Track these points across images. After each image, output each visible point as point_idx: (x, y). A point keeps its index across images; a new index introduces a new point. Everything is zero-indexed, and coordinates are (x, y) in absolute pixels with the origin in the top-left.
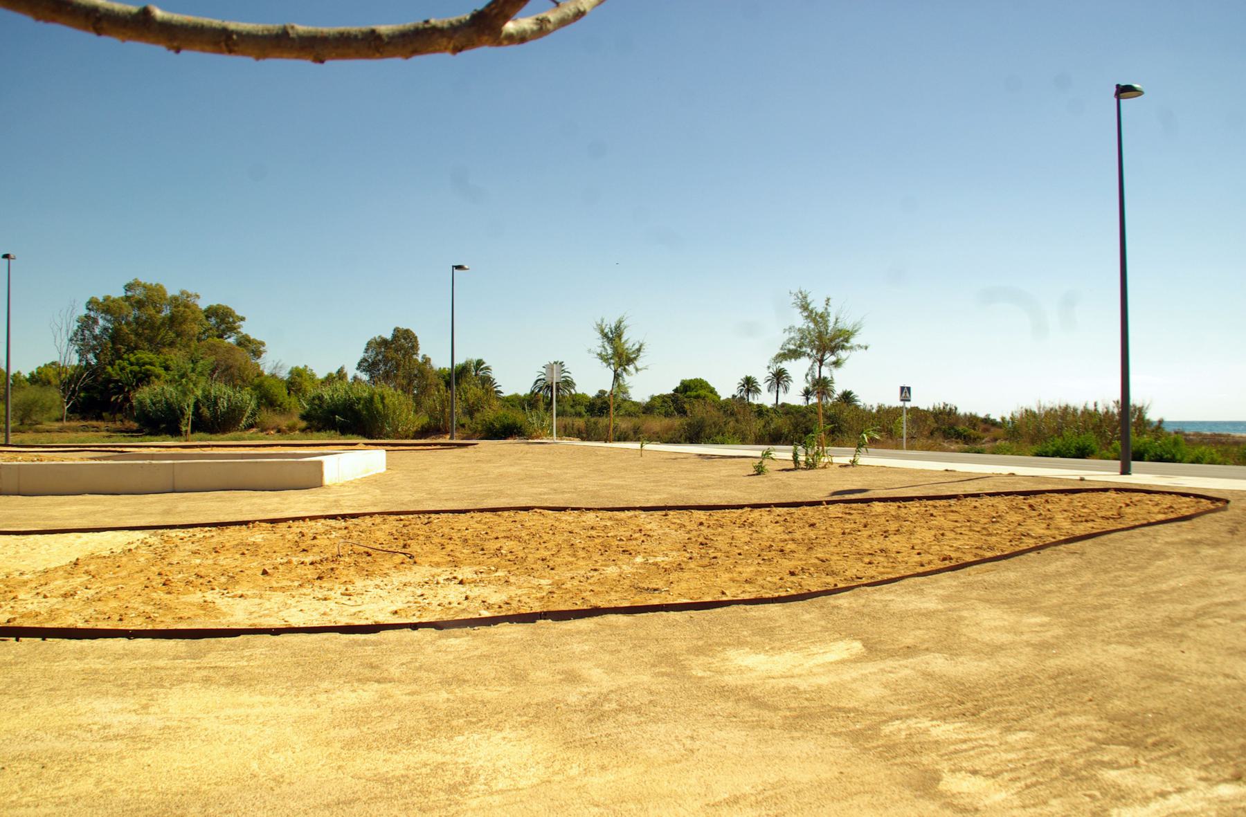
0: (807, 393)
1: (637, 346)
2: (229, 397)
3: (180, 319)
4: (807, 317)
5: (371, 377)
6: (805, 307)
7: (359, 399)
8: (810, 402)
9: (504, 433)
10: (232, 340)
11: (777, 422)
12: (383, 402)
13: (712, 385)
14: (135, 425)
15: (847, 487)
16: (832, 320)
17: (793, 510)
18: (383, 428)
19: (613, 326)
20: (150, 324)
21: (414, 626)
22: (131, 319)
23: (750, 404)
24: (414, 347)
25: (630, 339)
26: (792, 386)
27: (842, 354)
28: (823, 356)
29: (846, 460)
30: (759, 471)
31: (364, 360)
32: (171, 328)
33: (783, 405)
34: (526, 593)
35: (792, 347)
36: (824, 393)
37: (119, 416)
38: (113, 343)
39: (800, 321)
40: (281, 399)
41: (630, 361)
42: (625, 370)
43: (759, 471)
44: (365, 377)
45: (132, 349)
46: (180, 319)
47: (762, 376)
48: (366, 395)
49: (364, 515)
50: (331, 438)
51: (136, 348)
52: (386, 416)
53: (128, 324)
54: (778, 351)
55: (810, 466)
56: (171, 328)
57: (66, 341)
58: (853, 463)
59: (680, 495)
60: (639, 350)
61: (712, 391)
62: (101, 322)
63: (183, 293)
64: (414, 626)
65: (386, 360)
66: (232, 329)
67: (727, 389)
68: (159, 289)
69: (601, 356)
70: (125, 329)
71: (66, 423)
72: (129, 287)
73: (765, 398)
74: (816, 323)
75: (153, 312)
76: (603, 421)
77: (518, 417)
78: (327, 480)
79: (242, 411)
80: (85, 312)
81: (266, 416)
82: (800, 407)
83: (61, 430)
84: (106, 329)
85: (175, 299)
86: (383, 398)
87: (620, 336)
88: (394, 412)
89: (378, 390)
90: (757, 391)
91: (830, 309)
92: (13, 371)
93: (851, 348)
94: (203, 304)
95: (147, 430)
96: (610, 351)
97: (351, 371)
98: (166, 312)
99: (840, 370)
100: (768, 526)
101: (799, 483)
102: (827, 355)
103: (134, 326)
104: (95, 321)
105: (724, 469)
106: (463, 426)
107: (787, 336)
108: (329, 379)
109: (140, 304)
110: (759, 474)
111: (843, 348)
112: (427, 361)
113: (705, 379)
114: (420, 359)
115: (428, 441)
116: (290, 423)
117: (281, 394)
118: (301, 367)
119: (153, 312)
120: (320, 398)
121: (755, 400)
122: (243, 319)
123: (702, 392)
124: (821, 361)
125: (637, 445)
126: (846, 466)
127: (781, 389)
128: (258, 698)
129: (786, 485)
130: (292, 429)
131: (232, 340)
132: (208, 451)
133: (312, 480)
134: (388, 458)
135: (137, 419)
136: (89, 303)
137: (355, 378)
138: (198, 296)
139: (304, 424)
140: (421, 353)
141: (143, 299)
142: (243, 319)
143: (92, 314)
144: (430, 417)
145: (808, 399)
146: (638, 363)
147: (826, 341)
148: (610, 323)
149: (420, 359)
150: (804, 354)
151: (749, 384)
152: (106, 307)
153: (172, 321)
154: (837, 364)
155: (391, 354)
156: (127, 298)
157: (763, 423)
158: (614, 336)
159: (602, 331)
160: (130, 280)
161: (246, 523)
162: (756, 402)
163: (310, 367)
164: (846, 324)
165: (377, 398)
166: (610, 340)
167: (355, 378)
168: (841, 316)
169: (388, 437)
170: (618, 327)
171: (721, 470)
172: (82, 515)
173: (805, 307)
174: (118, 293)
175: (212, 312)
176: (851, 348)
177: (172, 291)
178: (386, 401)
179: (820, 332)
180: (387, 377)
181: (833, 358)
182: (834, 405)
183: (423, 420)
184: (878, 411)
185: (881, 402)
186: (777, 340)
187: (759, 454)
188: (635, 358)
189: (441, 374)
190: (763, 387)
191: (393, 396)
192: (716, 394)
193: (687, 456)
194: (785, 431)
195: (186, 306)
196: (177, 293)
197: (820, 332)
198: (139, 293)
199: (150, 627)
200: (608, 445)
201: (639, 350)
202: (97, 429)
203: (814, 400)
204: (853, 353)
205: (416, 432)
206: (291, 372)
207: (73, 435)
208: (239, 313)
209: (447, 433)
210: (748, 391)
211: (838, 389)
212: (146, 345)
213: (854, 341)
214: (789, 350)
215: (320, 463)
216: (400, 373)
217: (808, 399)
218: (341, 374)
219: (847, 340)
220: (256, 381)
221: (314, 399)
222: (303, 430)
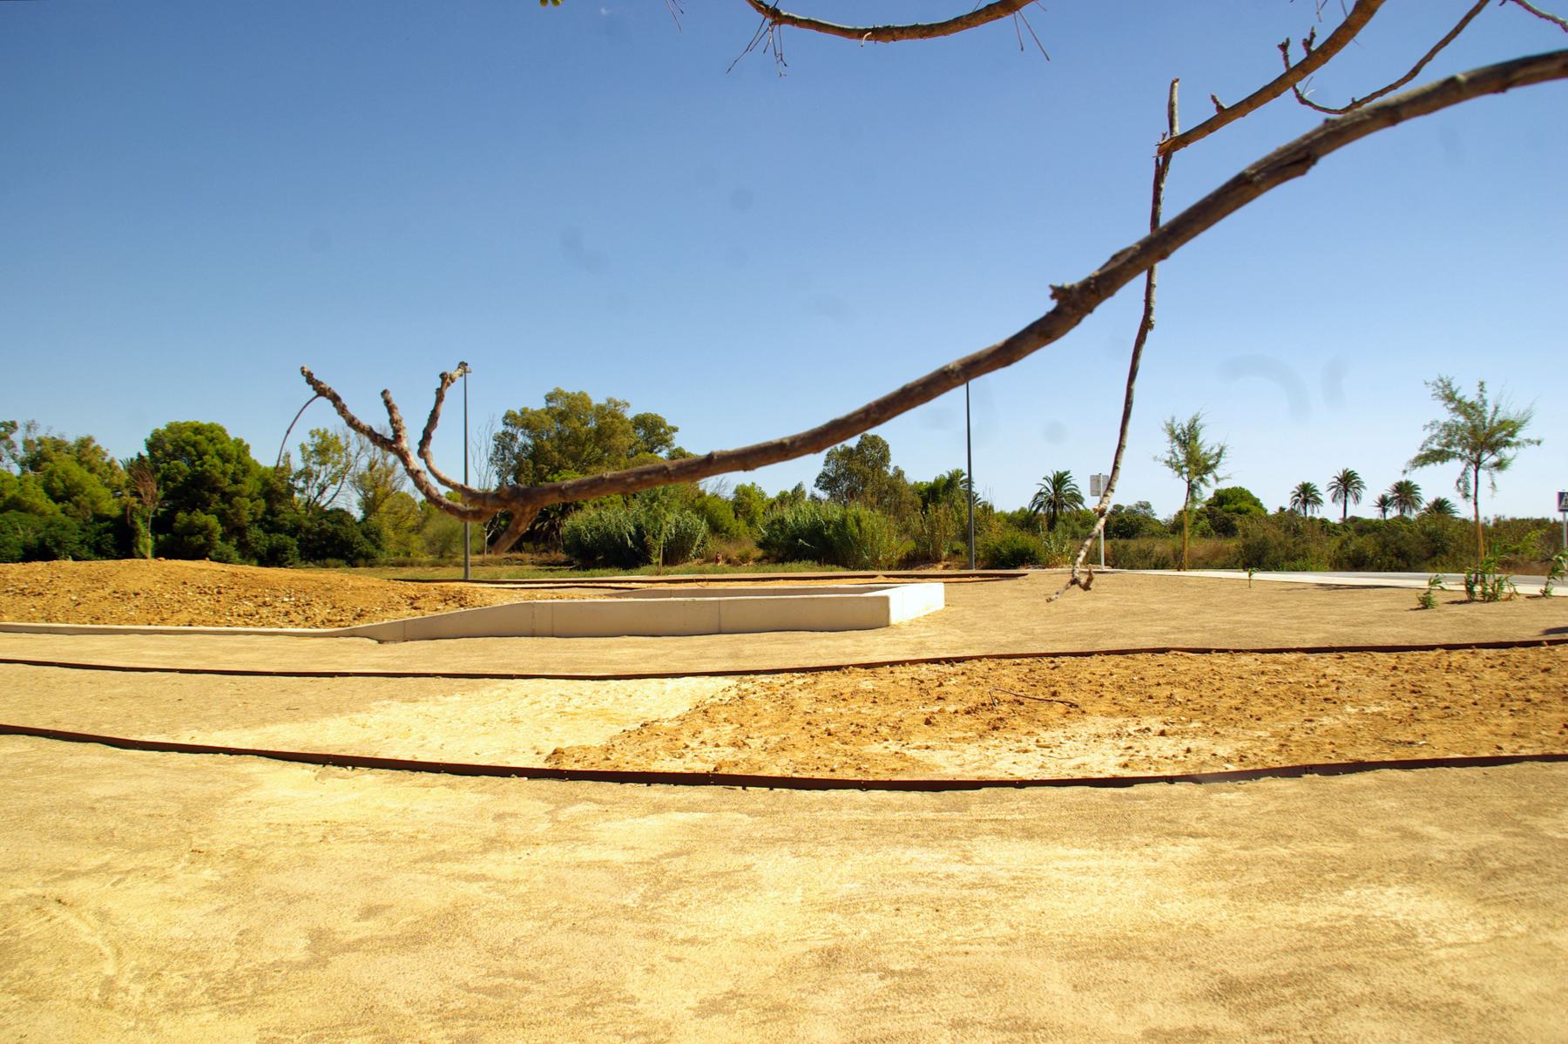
0: (1384, 503)
1: (1216, 450)
2: (678, 522)
3: (608, 432)
4: (1454, 410)
5: (832, 495)
6: (1450, 397)
7: (828, 523)
8: (1389, 516)
9: (1013, 560)
10: (664, 454)
11: (1357, 543)
12: (858, 525)
13: (1256, 495)
14: (562, 557)
15: (268, 639)
16: (1490, 409)
17: (1504, 651)
18: (859, 557)
19: (1185, 426)
20: (575, 439)
21: (1171, 780)
22: (552, 434)
23: (1312, 519)
24: (885, 457)
25: (1207, 442)
26: (1364, 494)
27: (1507, 452)
28: (1479, 456)
29: (1536, 590)
30: (1426, 603)
31: (824, 475)
32: (596, 444)
33: (1354, 519)
34: (1224, 750)
35: (1435, 447)
36: (1407, 503)
37: (542, 546)
38: (535, 463)
39: (1444, 414)
40: (727, 523)
41: (1208, 469)
42: (1202, 480)
43: (1426, 603)
44: (823, 495)
45: (556, 470)
46: (608, 432)
47: (1323, 483)
48: (837, 517)
49: (971, 658)
50: (811, 570)
51: (560, 467)
52: (864, 542)
53: (551, 440)
54: (1416, 453)
55: (1492, 598)
56: (596, 444)
57: (485, 461)
58: (1545, 594)
59: (1343, 634)
60: (1219, 455)
61: (1256, 503)
62: (521, 439)
63: (609, 401)
64: (1171, 780)
65: (848, 474)
66: (664, 442)
67: (1275, 498)
68: (583, 398)
69: (1170, 463)
70: (548, 446)
71: (488, 556)
72: (550, 398)
73: (1330, 511)
74: (1468, 416)
75: (578, 425)
76: (1133, 545)
77: (1025, 540)
78: (894, 618)
79: (692, 538)
80: (500, 428)
81: (713, 545)
82: (1378, 521)
83: (483, 564)
84: (525, 447)
85: (601, 408)
86: (858, 521)
87: (1195, 438)
88: (873, 537)
89: (852, 511)
90: (1318, 502)
91: (1486, 396)
92: (1481, 520)
93: (1518, 444)
94: (630, 414)
95: (577, 563)
96: (1181, 457)
97: (810, 488)
98: (593, 425)
99: (1504, 473)
100: (1489, 674)
101: (1493, 619)
102: (1485, 456)
103: (556, 442)
104: (513, 437)
105: (1377, 604)
106: (957, 553)
107: (1427, 434)
108: (783, 499)
109: (562, 417)
110: (1425, 608)
111: (1507, 444)
112: (899, 474)
113: (1246, 488)
114: (891, 472)
115: (914, 572)
116: (741, 551)
117: (728, 518)
118: (748, 484)
119: (578, 425)
120: (782, 521)
121: (1318, 513)
122: (675, 430)
123: (1244, 505)
124: (1478, 463)
125: (1245, 575)
126: (1536, 597)
127: (1350, 499)
128: (1061, 851)
129: (1475, 622)
130: (744, 559)
131: (664, 454)
132: (713, 586)
133: (877, 619)
134: (946, 592)
135: (567, 550)
136: (506, 417)
137: (812, 496)
138: (627, 405)
139: (759, 553)
140: (892, 464)
141: (566, 409)
142: (675, 430)
143: (510, 429)
144: (917, 542)
145: (1384, 511)
146: (1218, 472)
147: (1481, 438)
148: (1183, 422)
149: (891, 472)
150: (1454, 455)
151: (1307, 494)
152: (525, 421)
153: (600, 435)
154: (1500, 465)
155: (856, 466)
156: (549, 411)
157: (1338, 543)
158: (1187, 439)
159: (1172, 432)
160: (551, 390)
161: (838, 668)
162: (1318, 516)
163: (759, 484)
164: (1509, 411)
165: (851, 521)
166: (1184, 444)
167: (812, 496)
168: (1502, 402)
169: (866, 569)
170: (1192, 427)
171: (1385, 601)
172: (647, 659)
173: (1450, 397)
174: (538, 404)
175: (640, 422)
176: (1518, 444)
177: (598, 399)
178: (863, 524)
179: (1475, 427)
180: (852, 493)
181: (1494, 459)
182: (1421, 517)
183: (910, 545)
184: (1496, 525)
185: (1500, 513)
186: (1416, 440)
187: (1424, 584)
188: (1214, 466)
189: (917, 489)
190: (1326, 496)
191: (868, 517)
192: (1261, 506)
193: (1305, 587)
194: (1370, 553)
195: (615, 416)
196: (603, 402)
197: (1475, 427)
198: (558, 405)
199: (859, 778)
200: (1182, 573)
201: (1219, 455)
202: (521, 562)
203: (1393, 513)
204: (1521, 450)
205: (900, 560)
206: (736, 491)
207: (497, 569)
208: (669, 423)
209: (938, 561)
210: (1305, 502)
211: (1427, 497)
212: (570, 464)
213: (1521, 435)
214: (1433, 452)
215: (886, 599)
216: (868, 489)
217: (1384, 511)
218: (798, 492)
219: (1512, 434)
220: (698, 503)
221: (773, 523)
222: (758, 560)
